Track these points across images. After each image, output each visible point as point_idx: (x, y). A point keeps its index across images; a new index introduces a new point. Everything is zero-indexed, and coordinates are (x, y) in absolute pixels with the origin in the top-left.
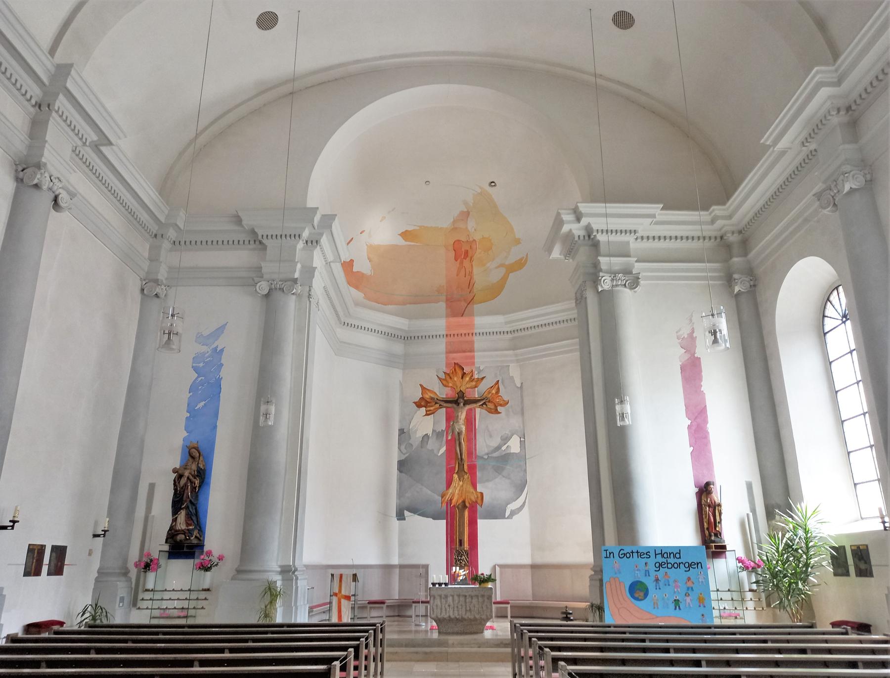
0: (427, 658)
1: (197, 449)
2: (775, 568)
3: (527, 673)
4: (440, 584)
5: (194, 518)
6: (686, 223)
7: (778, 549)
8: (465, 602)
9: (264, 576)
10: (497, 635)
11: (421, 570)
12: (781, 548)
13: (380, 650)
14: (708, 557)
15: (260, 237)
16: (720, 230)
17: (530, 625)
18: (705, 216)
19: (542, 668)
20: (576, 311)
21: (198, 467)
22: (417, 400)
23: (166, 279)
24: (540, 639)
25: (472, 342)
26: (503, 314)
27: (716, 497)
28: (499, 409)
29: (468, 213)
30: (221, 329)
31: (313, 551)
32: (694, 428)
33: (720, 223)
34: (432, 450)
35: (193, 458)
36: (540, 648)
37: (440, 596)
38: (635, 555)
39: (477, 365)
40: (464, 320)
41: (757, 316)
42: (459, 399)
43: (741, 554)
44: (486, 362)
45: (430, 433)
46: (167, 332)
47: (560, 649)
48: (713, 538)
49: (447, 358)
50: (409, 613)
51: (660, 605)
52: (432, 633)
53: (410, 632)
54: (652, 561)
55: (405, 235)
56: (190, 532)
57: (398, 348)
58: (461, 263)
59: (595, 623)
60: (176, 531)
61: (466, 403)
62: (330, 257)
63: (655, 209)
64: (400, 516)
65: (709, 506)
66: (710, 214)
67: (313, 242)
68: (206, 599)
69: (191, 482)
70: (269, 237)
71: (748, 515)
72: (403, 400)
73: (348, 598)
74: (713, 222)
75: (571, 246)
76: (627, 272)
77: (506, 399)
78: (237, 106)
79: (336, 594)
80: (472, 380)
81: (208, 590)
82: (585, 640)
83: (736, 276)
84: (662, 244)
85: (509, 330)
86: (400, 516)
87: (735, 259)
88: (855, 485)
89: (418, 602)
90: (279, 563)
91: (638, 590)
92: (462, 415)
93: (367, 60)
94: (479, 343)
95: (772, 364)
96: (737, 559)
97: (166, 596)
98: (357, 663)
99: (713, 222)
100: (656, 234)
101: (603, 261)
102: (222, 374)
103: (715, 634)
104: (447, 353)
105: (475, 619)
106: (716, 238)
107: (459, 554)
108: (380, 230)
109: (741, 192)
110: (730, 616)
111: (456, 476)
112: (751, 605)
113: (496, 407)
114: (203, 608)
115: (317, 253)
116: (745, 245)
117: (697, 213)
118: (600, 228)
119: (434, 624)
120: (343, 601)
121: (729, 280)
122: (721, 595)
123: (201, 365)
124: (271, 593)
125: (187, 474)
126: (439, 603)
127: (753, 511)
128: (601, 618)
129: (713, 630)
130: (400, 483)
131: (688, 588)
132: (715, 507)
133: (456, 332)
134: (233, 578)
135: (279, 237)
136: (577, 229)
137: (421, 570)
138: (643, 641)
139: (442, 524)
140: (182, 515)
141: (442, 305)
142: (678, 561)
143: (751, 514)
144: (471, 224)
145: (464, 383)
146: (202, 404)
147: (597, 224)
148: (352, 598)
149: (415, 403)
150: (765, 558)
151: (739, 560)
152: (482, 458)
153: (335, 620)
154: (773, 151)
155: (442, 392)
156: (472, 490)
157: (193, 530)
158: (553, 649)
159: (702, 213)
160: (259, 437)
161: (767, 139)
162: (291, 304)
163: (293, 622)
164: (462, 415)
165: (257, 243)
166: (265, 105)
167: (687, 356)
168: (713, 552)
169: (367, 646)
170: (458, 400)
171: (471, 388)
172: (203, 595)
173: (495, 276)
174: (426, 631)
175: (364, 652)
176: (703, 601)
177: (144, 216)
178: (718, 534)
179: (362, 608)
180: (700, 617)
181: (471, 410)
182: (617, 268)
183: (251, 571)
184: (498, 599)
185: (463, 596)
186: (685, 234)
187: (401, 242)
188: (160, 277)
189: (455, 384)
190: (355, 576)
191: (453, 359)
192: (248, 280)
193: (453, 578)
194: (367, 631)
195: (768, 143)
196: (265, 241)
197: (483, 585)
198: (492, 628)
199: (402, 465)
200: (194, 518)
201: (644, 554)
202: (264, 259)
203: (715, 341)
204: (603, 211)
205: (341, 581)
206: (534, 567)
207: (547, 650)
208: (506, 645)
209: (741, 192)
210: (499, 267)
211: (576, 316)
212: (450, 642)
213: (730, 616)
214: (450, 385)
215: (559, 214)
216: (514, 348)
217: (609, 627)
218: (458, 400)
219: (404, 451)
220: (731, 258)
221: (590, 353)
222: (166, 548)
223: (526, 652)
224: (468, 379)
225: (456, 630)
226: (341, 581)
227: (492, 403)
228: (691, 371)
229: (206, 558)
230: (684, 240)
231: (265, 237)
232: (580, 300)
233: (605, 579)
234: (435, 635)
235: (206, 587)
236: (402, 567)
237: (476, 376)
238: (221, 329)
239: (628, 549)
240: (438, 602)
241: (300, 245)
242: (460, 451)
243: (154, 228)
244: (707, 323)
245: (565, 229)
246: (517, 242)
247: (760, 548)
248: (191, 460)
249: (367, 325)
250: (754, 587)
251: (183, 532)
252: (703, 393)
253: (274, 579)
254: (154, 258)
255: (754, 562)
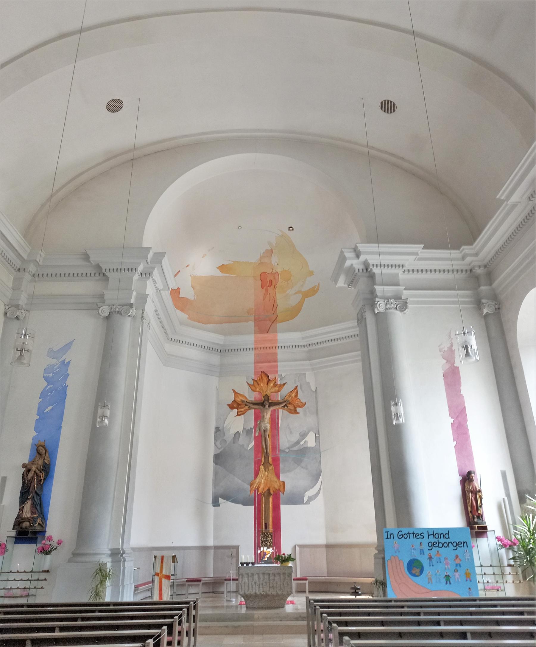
0: (235, 631)
1: (43, 446)
2: (528, 546)
3: (320, 645)
4: (248, 564)
5: (38, 508)
6: (443, 259)
7: (529, 528)
8: (269, 580)
9: (96, 559)
10: (297, 609)
11: (232, 551)
12: (532, 528)
13: (193, 625)
14: (472, 536)
15: (104, 271)
16: (470, 265)
17: (323, 601)
18: (455, 254)
19: (331, 640)
20: (358, 329)
21: (44, 463)
22: (230, 402)
23: (26, 304)
24: (330, 614)
25: (276, 354)
26: (301, 330)
27: (477, 484)
28: (298, 409)
29: (272, 251)
30: (69, 345)
31: (140, 535)
32: (456, 425)
33: (469, 259)
34: (243, 445)
35: (40, 454)
36: (330, 623)
37: (248, 574)
38: (411, 535)
39: (279, 373)
40: (269, 336)
41: (503, 333)
42: (265, 402)
43: (499, 533)
44: (287, 370)
45: (241, 430)
46: (19, 349)
47: (346, 624)
48: (476, 520)
49: (255, 367)
50: (221, 590)
51: (434, 580)
52: (241, 608)
53: (222, 607)
54: (425, 541)
55: (222, 268)
56: (34, 520)
57: (215, 359)
58: (267, 290)
59: (379, 598)
60: (22, 519)
61: (271, 405)
62: (160, 286)
63: (418, 248)
64: (216, 503)
65: (472, 492)
66: (461, 252)
67: (147, 274)
68: (45, 580)
69: (37, 476)
70: (111, 270)
71: (504, 499)
72: (219, 403)
73: (168, 577)
74: (463, 258)
75: (353, 277)
76: (398, 297)
77: (303, 401)
78: (87, 171)
79: (157, 574)
80: (275, 385)
81: (48, 571)
82: (369, 614)
83: (484, 301)
84: (420, 276)
85: (305, 344)
86: (216, 503)
87: (483, 288)
88: (429, 535)
89: (229, 580)
90: (110, 547)
91: (414, 567)
92: (268, 416)
93: (173, 139)
94: (281, 354)
95: (516, 372)
96: (497, 538)
97: (12, 577)
98: (170, 638)
99: (463, 258)
100: (420, 268)
101: (378, 289)
102: (68, 382)
103: (480, 606)
104: (255, 363)
105: (278, 595)
106: (466, 271)
107: (265, 536)
108: (201, 265)
109: (484, 236)
110: (493, 588)
111: (262, 468)
112: (510, 578)
113: (295, 408)
114: (42, 588)
115: (149, 284)
116: (490, 277)
117: (448, 251)
118: (375, 263)
119: (243, 599)
120: (163, 580)
121: (478, 304)
122: (484, 570)
123: (51, 375)
124: (101, 574)
125: (34, 468)
126: (247, 580)
127: (508, 495)
128: (385, 593)
129: (478, 602)
130: (216, 474)
131: (457, 565)
132: (477, 492)
133: (262, 346)
134: (69, 561)
135: (119, 270)
136: (357, 264)
137: (232, 551)
138: (418, 614)
139: (250, 510)
140: (28, 505)
141: (252, 324)
142: (448, 541)
143: (506, 499)
144: (274, 259)
145: (269, 388)
146: (50, 408)
147: (373, 260)
148: (172, 577)
149: (228, 405)
150: (519, 537)
151: (499, 539)
152: (284, 451)
153: (156, 599)
154: (507, 205)
155: (251, 396)
156: (275, 479)
157: (37, 518)
158: (340, 623)
159: (451, 251)
160: (96, 436)
161: (501, 195)
162: (127, 325)
163: (120, 600)
164: (268, 416)
165: (101, 275)
166: (111, 168)
167: (448, 366)
168: (476, 532)
169: (180, 623)
170: (264, 403)
171: (275, 392)
172: (43, 576)
173: (294, 301)
174: (237, 607)
175: (177, 628)
176: (469, 576)
177: (11, 255)
178: (480, 516)
179: (182, 585)
180: (468, 590)
181: (275, 410)
182: (389, 294)
183: (82, 555)
184: (299, 576)
185: (265, 573)
186: (442, 268)
187: (219, 273)
188: (20, 303)
189: (261, 388)
190: (174, 557)
191: (260, 368)
192: (93, 304)
193: (260, 558)
194: (181, 609)
195: (502, 198)
196: (107, 274)
197: (284, 564)
198: (292, 602)
199: (217, 458)
200: (38, 508)
201: (419, 535)
202: (106, 287)
203: (467, 355)
204: (376, 250)
205: (162, 562)
206: (328, 546)
207: (335, 625)
208: (303, 619)
209: (484, 236)
210: (296, 293)
211: (358, 332)
212: (256, 616)
213: (493, 588)
214: (258, 390)
215: (342, 252)
216: (310, 359)
217: (390, 601)
218: (264, 403)
219: (219, 446)
220: (479, 287)
221: (370, 363)
222: (13, 534)
223: (318, 626)
224: (272, 384)
225: (261, 605)
226: (162, 562)
227: (292, 405)
228: (452, 378)
229: (47, 543)
230: (442, 273)
231: (108, 271)
232: (361, 320)
233: (387, 558)
234: (244, 610)
235: (46, 569)
236: (216, 548)
237: (279, 382)
238: (69, 345)
239: (405, 531)
240: (246, 580)
241: (136, 276)
242: (266, 445)
243: (18, 263)
244: (459, 340)
245: (348, 263)
246: (311, 273)
247: (515, 528)
248: (38, 456)
249: (190, 341)
250: (512, 562)
251: (28, 520)
252: (462, 397)
253: (105, 561)
254: (16, 288)
255: (511, 541)
